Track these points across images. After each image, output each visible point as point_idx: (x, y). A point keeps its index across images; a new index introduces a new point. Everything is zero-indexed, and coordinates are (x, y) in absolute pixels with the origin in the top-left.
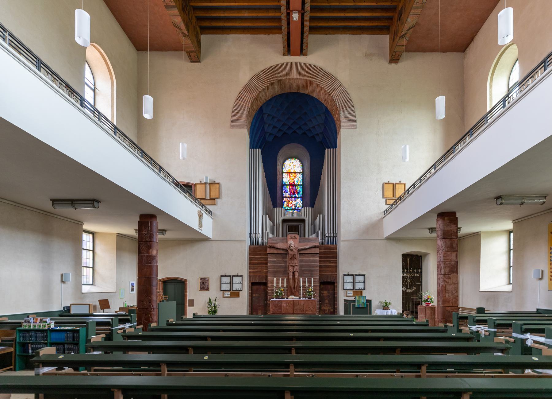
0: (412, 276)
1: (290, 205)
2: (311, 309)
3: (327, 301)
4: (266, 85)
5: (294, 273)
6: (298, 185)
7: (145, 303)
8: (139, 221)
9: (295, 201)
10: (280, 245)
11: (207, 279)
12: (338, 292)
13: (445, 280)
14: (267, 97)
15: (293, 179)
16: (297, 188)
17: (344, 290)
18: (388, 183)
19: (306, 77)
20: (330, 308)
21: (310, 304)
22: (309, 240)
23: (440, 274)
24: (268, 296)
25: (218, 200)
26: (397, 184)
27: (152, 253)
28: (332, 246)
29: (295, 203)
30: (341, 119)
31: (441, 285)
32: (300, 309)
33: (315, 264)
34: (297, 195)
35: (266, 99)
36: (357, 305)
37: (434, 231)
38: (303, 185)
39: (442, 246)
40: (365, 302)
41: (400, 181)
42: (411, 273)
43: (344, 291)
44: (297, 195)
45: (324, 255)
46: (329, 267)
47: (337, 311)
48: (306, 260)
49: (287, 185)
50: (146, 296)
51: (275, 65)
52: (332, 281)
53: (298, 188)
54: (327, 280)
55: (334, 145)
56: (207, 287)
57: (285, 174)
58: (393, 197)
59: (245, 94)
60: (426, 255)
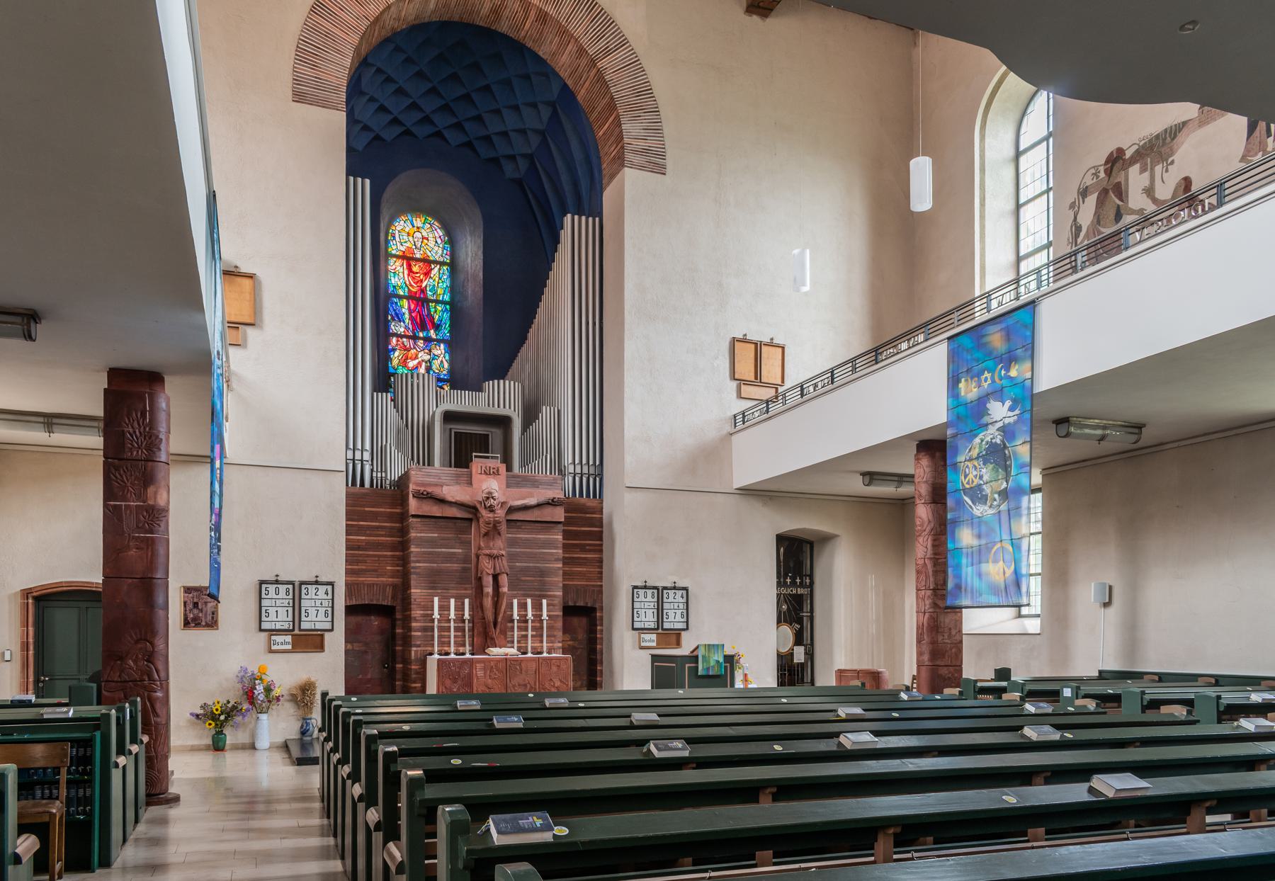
0: (790, 594)
1: (411, 364)
2: (556, 685)
5: (495, 577)
6: (437, 302)
7: (131, 663)
8: (105, 389)
9: (427, 351)
10: (453, 492)
13: (936, 602)
14: (401, 22)
15: (421, 281)
16: (432, 310)
17: (634, 629)
18: (744, 340)
21: (554, 669)
22: (536, 481)
23: (924, 588)
24: (414, 649)
25: (249, 330)
27: (155, 498)
28: (591, 503)
29: (427, 357)
30: (626, 140)
31: (927, 615)
32: (525, 685)
33: (552, 554)
34: (432, 333)
35: (396, 26)
36: (703, 669)
37: (876, 479)
38: (451, 303)
39: (930, 522)
40: (721, 660)
41: (772, 339)
42: (789, 586)
43: (634, 632)
44: (432, 333)
46: (580, 565)
48: (527, 540)
49: (401, 297)
50: (137, 642)
52: (589, 605)
53: (436, 312)
54: (575, 602)
55: (589, 204)
56: (209, 618)
57: (395, 259)
58: (756, 378)
60: (826, 539)
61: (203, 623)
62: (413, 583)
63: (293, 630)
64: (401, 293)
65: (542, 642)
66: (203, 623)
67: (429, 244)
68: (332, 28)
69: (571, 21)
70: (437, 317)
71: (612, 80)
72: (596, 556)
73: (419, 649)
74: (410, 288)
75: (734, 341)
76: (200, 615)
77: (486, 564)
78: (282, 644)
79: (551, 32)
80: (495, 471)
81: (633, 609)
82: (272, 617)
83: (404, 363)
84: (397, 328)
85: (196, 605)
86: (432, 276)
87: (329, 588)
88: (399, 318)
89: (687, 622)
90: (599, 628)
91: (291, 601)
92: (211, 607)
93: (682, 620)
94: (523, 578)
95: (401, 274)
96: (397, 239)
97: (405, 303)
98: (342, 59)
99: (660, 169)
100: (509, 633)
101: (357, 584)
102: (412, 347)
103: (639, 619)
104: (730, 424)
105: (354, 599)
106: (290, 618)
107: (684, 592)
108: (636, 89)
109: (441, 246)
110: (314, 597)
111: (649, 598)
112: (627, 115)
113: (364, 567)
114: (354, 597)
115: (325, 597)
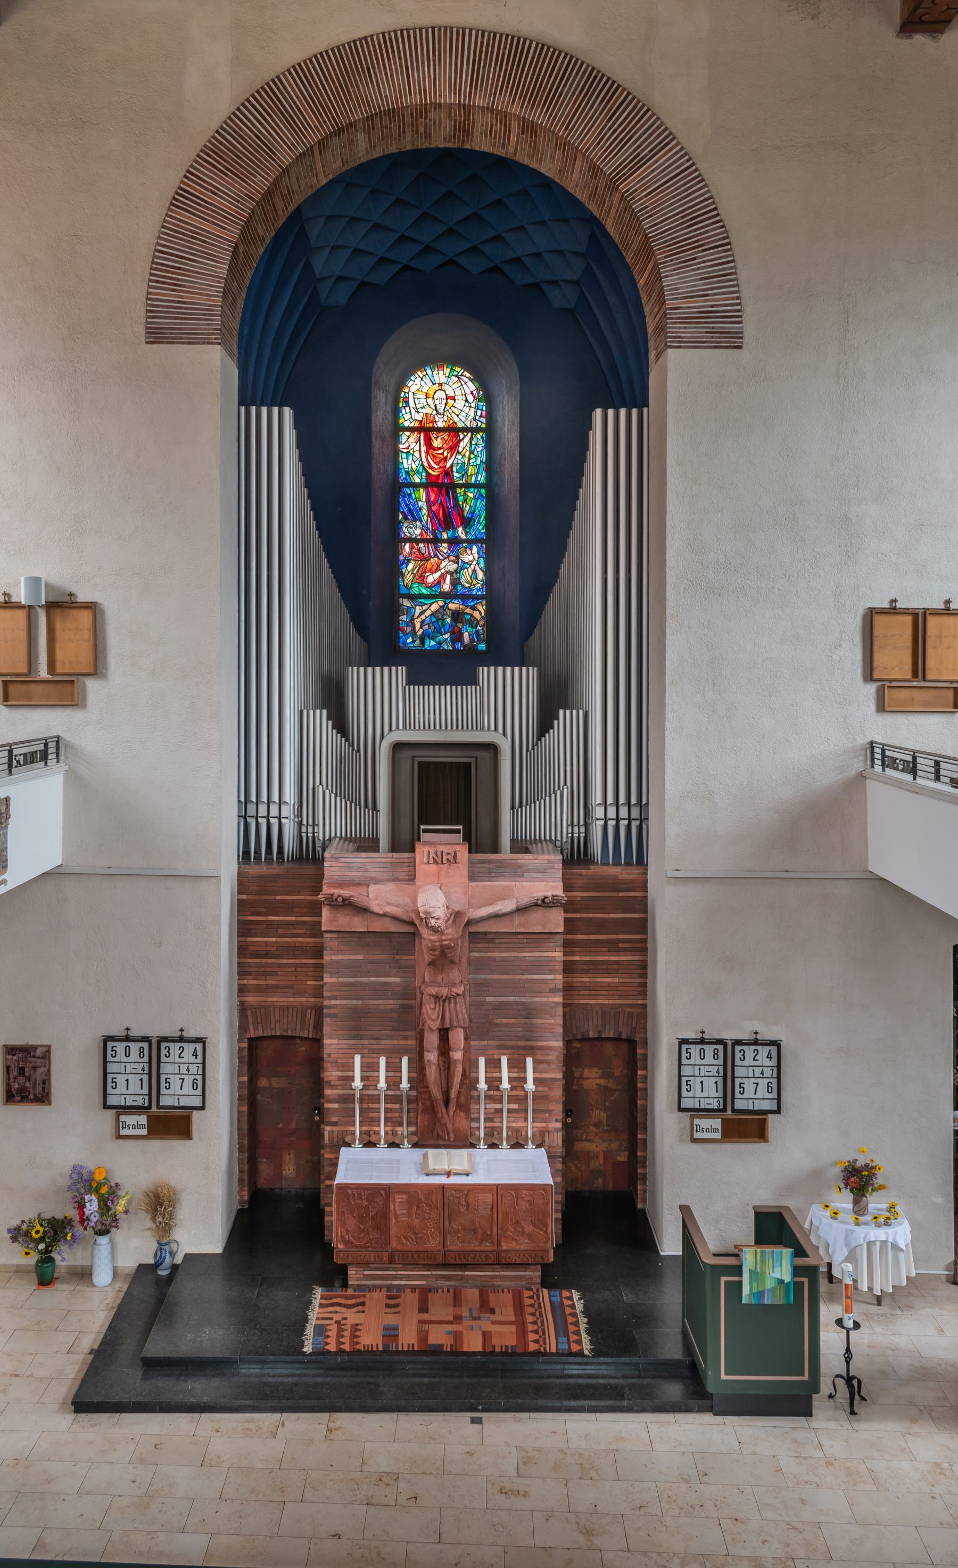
1: (431, 579)
3: (599, 1115)
4: (314, 138)
5: (444, 1033)
6: (467, 486)
9: (453, 558)
11: (39, 1052)
12: (653, 1089)
15: (445, 459)
16: (461, 499)
17: (681, 1110)
18: (893, 610)
19: (502, 102)
20: (615, 1146)
26: (936, 613)
29: (453, 567)
32: (475, 1231)
36: (751, 1294)
40: (787, 1278)
41: (948, 602)
43: (681, 1114)
45: (584, 916)
46: (608, 972)
47: (644, 1175)
48: (504, 960)
49: (416, 486)
51: (354, 42)
53: (465, 500)
56: (39, 1089)
57: (408, 433)
58: (915, 675)
59: (213, 180)
61: (32, 1097)
62: (326, 1030)
63: (150, 1107)
64: (417, 480)
65: (526, 1120)
66: (32, 1097)
67: (455, 405)
68: (201, 223)
69: (574, 126)
70: (468, 507)
71: (646, 207)
72: (636, 958)
73: (336, 1128)
74: (430, 471)
75: (871, 614)
76: (28, 1084)
77: (430, 1012)
78: (708, 1130)
79: (548, 145)
80: (451, 859)
81: (680, 1076)
82: (121, 1088)
83: (421, 579)
84: (411, 530)
85: (22, 1071)
86: (460, 449)
87: (199, 1046)
88: (414, 515)
89: (779, 1099)
90: (640, 1072)
91: (146, 1066)
92: (41, 1074)
93: (770, 1096)
94: (498, 1021)
95: (417, 454)
96: (412, 404)
97: (422, 493)
98: (215, 266)
99: (734, 341)
100: (473, 1106)
101: (265, 1007)
102: (432, 554)
103: (690, 1094)
104: (862, 758)
105: (260, 1029)
106: (145, 1090)
107: (774, 1049)
108: (688, 214)
109: (473, 405)
110: (178, 1060)
111: (709, 1059)
112: (672, 260)
113: (274, 982)
114: (260, 1026)
115: (193, 1059)
